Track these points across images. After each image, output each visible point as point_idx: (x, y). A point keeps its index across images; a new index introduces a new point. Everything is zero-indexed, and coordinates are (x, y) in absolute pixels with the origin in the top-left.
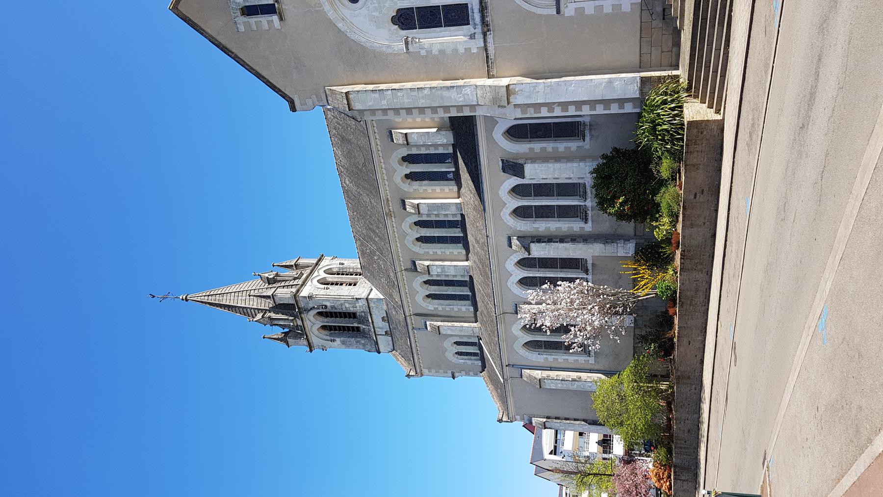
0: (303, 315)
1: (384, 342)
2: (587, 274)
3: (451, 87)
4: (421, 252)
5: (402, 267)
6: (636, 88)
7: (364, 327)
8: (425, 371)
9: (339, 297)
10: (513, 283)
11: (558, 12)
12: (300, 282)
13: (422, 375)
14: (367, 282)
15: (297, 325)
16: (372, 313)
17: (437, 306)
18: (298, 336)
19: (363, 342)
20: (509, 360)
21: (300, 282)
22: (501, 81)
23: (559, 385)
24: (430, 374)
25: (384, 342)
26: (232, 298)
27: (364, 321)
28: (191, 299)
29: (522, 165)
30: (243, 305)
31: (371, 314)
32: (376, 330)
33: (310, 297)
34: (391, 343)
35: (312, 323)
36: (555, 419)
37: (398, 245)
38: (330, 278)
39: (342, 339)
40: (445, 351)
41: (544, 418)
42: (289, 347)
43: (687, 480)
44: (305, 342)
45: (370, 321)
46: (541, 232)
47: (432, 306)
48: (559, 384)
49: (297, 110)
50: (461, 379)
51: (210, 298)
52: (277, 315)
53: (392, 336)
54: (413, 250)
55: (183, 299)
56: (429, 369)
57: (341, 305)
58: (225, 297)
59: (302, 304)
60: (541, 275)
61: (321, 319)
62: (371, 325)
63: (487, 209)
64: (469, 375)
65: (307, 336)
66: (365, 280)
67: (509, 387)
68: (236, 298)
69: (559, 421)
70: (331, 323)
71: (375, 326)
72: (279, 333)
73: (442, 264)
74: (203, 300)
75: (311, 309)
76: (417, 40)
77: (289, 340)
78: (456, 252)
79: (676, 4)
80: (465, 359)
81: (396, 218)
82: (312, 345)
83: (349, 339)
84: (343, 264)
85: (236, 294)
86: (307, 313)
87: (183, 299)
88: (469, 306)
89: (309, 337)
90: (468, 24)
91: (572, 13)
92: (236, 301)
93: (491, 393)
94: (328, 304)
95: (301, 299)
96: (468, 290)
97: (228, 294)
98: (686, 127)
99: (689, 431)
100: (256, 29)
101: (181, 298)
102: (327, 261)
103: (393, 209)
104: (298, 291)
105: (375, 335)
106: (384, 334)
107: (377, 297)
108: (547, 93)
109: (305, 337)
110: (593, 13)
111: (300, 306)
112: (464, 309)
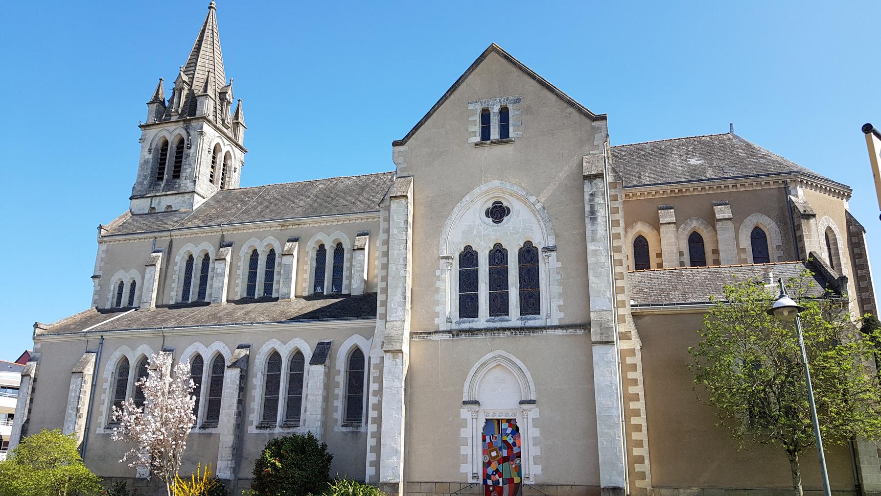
1: (142, 205)
2: (200, 428)
4: (241, 254)
6: (389, 478)
8: (104, 247)
9: (199, 163)
11: (465, 403)
12: (219, 125)
13: (100, 243)
14: (213, 194)
16: (177, 196)
17: (178, 265)
19: (145, 182)
20: (110, 339)
21: (219, 125)
23: (73, 394)
25: (142, 205)
26: (208, 54)
27: (169, 186)
28: (211, 12)
29: (324, 363)
31: (176, 194)
33: (201, 133)
38: (220, 157)
39: (151, 161)
40: (126, 270)
41: (35, 375)
42: (147, 104)
44: (150, 122)
45: (169, 193)
47: (179, 260)
48: (75, 394)
50: (90, 287)
51: (210, 32)
52: (184, 97)
53: (148, 214)
56: (106, 251)
58: (209, 46)
59: (194, 124)
62: (163, 194)
63: (282, 325)
67: (76, 338)
68: (207, 58)
69: (30, 392)
71: (162, 197)
72: (164, 96)
75: (188, 133)
76: (449, 268)
77: (155, 105)
80: (114, 291)
81: (279, 231)
82: (147, 128)
84: (235, 171)
87: (211, 4)
88: (176, 300)
91: (462, 416)
93: (70, 318)
94: (192, 151)
95: (200, 123)
96: (194, 300)
97: (212, 50)
100: (469, 120)
102: (240, 156)
103: (289, 229)
104: (209, 121)
106: (152, 206)
111: (192, 122)
112: (173, 294)
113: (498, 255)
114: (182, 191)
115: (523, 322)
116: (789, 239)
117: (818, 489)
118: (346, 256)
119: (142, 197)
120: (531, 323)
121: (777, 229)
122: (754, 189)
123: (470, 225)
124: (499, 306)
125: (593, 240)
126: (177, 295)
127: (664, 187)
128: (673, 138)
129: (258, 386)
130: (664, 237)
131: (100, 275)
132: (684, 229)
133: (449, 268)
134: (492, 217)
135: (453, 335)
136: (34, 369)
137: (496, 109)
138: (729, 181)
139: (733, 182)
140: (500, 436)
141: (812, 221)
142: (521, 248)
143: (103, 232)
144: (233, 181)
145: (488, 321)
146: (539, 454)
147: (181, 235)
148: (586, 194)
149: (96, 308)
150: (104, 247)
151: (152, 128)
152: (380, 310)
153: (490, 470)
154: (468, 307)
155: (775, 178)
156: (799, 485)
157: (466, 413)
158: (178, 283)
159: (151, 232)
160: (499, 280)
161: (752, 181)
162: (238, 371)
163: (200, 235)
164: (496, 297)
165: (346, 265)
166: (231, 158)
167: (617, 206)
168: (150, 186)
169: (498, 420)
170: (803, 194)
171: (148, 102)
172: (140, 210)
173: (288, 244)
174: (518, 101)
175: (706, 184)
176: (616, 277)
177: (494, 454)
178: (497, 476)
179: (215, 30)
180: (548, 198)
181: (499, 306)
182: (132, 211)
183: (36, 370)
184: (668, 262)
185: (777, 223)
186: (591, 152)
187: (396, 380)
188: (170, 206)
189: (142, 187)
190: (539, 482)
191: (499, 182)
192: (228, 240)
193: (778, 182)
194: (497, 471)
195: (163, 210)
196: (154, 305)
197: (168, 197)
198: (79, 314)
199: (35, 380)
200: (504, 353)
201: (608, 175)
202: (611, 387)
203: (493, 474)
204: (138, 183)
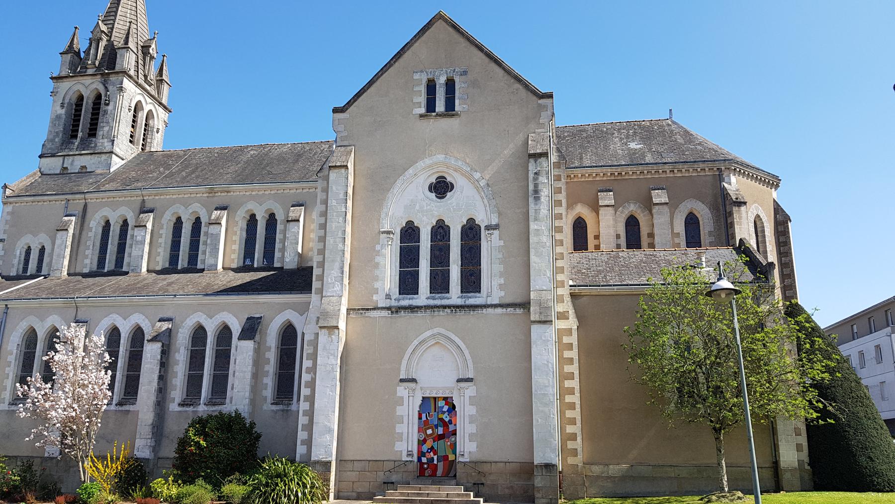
1: (53, 164)
5: (147, 197)
6: (321, 457)
8: (9, 208)
9: (118, 121)
10: (114, 320)
11: (402, 381)
13: (4, 203)
15: (87, 68)
16: (93, 155)
19: (57, 140)
20: (13, 308)
21: (141, 81)
24: (5, 214)
25: (53, 164)
27: (84, 145)
31: (91, 154)
33: (121, 89)
38: (142, 116)
42: (60, 54)
45: (83, 152)
52: (103, 48)
53: (60, 174)
56: (12, 213)
62: (77, 153)
73: (146, 242)
76: (390, 243)
79: (397, 494)
80: (20, 257)
81: (206, 198)
84: (158, 132)
85: (134, 8)
94: (110, 108)
95: (120, 78)
96: (110, 269)
102: (163, 116)
104: (130, 77)
112: (87, 261)
113: (440, 231)
115: (464, 299)
117: (739, 465)
118: (280, 227)
119: (53, 155)
121: (710, 215)
124: (440, 284)
130: (603, 219)
131: (4, 239)
132: (621, 213)
133: (390, 243)
134: (436, 192)
138: (666, 166)
139: (671, 167)
141: (743, 208)
143: (8, 192)
146: (475, 432)
151: (65, 81)
152: (315, 285)
154: (408, 284)
155: (710, 165)
157: (402, 391)
159: (63, 194)
160: (440, 256)
162: (159, 345)
163: (118, 199)
164: (437, 274)
165: (279, 236)
169: (435, 398)
170: (736, 182)
171: (61, 52)
173: (216, 212)
174: (465, 73)
177: (429, 432)
178: (432, 453)
181: (440, 284)
182: (42, 170)
184: (606, 245)
186: (536, 130)
189: (53, 144)
190: (474, 459)
191: (443, 156)
192: (149, 205)
193: (713, 169)
194: (432, 448)
196: (66, 273)
202: (548, 366)
203: (427, 452)
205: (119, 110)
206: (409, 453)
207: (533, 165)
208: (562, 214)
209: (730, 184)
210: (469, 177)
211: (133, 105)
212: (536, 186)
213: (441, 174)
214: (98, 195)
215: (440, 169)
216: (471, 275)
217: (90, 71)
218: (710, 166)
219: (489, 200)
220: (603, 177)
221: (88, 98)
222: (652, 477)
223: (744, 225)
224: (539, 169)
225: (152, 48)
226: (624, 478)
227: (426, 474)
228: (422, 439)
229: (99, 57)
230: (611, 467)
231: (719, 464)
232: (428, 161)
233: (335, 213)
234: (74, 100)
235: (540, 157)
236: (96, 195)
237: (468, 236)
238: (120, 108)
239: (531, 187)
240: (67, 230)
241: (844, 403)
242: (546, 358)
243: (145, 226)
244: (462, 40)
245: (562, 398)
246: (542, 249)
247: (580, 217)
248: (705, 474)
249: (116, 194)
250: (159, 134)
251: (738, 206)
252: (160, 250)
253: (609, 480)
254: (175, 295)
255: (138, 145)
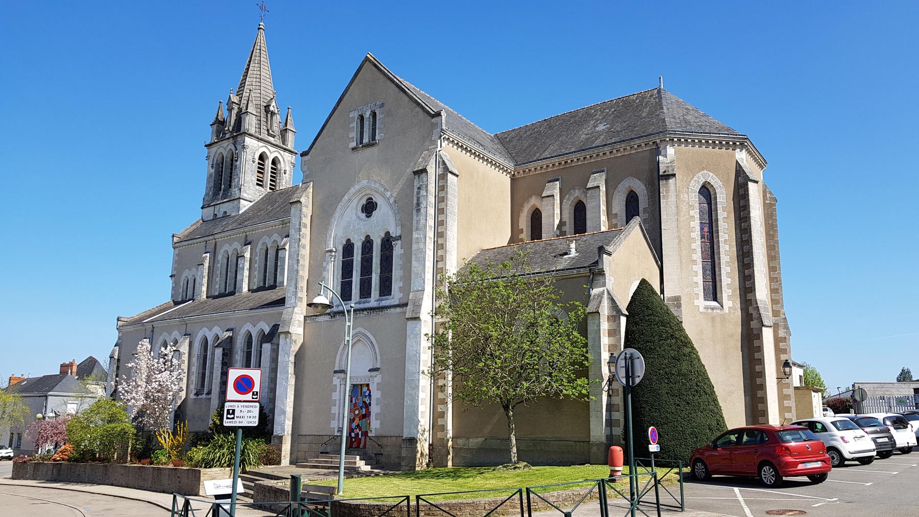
0: (231, 139)
1: (209, 212)
2: (206, 394)
3: (296, 287)
4: (258, 250)
6: (279, 432)
7: (221, 194)
8: (177, 251)
9: (243, 172)
11: (336, 372)
12: (264, 136)
13: (174, 248)
14: (261, 197)
15: (226, 134)
16: (230, 202)
17: (220, 262)
18: (218, 132)
19: (210, 194)
20: (157, 327)
21: (264, 136)
22: (299, 326)
24: (175, 255)
25: (209, 212)
26: (255, 72)
27: (225, 196)
28: (259, 33)
29: (270, 341)
30: (247, 83)
31: (229, 201)
32: (218, 206)
33: (244, 147)
34: (209, 219)
35: (225, 147)
36: (117, 366)
37: (263, 230)
38: (268, 164)
39: (214, 174)
41: (118, 357)
42: (211, 125)
43: (53, 474)
44: (213, 141)
45: (225, 200)
46: (235, 357)
49: (303, 157)
50: (170, 283)
51: (258, 51)
52: (235, 115)
53: (223, 217)
54: (260, 243)
55: (260, 25)
57: (237, 175)
58: (256, 65)
59: (239, 139)
60: (208, 356)
61: (229, 156)
62: (221, 202)
63: (252, 311)
64: (172, 290)
65: (217, 142)
66: (263, 195)
67: (139, 327)
68: (255, 76)
69: (115, 369)
70: (225, 165)
72: (224, 116)
73: (246, 268)
74: (256, 44)
75: (236, 147)
76: (333, 260)
77: (216, 125)
78: (256, 280)
79: (314, 461)
80: (183, 287)
82: (211, 147)
83: (213, 180)
84: (285, 173)
85: (258, 76)
86: (233, 144)
87: (260, 25)
88: (257, 285)
89: (215, 145)
90: (380, 296)
91: (334, 383)
92: (251, 76)
93: (149, 310)
94: (238, 163)
95: (243, 138)
96: (230, 291)
97: (259, 68)
98: (124, 465)
99: (79, 475)
100: (350, 127)
101: (261, 24)
102: (289, 159)
104: (251, 135)
105: (214, 205)
106: (215, 213)
107: (241, 206)
108: (283, 363)
109: (216, 141)
110: (333, 399)
112: (217, 286)
113: (368, 244)
114: (232, 198)
115: (379, 302)
116: (655, 200)
117: (567, 439)
120: (383, 303)
121: (646, 192)
122: (629, 153)
123: (349, 221)
124: (365, 292)
125: (417, 229)
126: (220, 287)
127: (553, 160)
128: (559, 113)
129: (238, 361)
130: (545, 210)
131: (175, 275)
132: (568, 200)
133: (333, 260)
135: (331, 317)
136: (117, 352)
137: (367, 115)
138: (606, 149)
139: (610, 149)
140: (361, 397)
141: (671, 181)
142: (384, 238)
143: (176, 239)
144: (284, 181)
145: (377, 300)
146: (379, 412)
147: (221, 238)
148: (415, 187)
149: (173, 301)
150: (177, 251)
153: (354, 425)
154: (346, 294)
155: (645, 140)
156: (512, 436)
157: (336, 380)
158: (220, 277)
159: (203, 237)
161: (626, 145)
162: (221, 349)
164: (365, 282)
166: (280, 162)
167: (444, 195)
168: (213, 197)
169: (361, 385)
170: (674, 153)
171: (211, 123)
172: (207, 217)
173: (285, 239)
174: (382, 105)
175: (587, 154)
176: (438, 259)
177: (357, 412)
178: (358, 430)
179: (262, 48)
180: (399, 192)
181: (365, 292)
182: (203, 218)
183: (118, 353)
184: (546, 234)
185: (645, 185)
186: (430, 147)
187: (286, 356)
188: (225, 212)
190: (378, 434)
191: (367, 181)
192: (249, 239)
193: (649, 143)
194: (358, 426)
195: (222, 216)
196: (205, 297)
197: (224, 204)
198: (157, 307)
199: (118, 360)
200: (362, 330)
201: (439, 167)
202: (416, 356)
203: (355, 428)
204: (207, 194)
205: (244, 164)
206: (340, 429)
207: (417, 181)
208: (443, 220)
209: (665, 156)
210: (383, 196)
211: (257, 157)
212: (418, 199)
213: (369, 196)
214: (225, 234)
215: (367, 192)
216: (386, 281)
217: (227, 136)
218: (646, 141)
219: (395, 214)
220: (547, 169)
221: (226, 157)
222: (500, 449)
223: (672, 197)
224: (421, 184)
225: (272, 106)
226: (481, 450)
227: (354, 447)
228: (352, 418)
229: (232, 124)
230: (471, 440)
231: (509, 439)
232: (357, 187)
233: (293, 241)
234: (220, 159)
235: (422, 173)
236: (223, 234)
237: (385, 248)
238: (244, 162)
239: (415, 202)
240: (203, 264)
241: (649, 380)
242: (415, 349)
243: (244, 256)
244: (381, 76)
245: (436, 381)
246: (420, 255)
247: (580, 200)
248: (538, 447)
249: (231, 233)
250: (287, 174)
251: (665, 179)
252: (256, 273)
253: (469, 452)
254: (234, 311)
255: (266, 187)
